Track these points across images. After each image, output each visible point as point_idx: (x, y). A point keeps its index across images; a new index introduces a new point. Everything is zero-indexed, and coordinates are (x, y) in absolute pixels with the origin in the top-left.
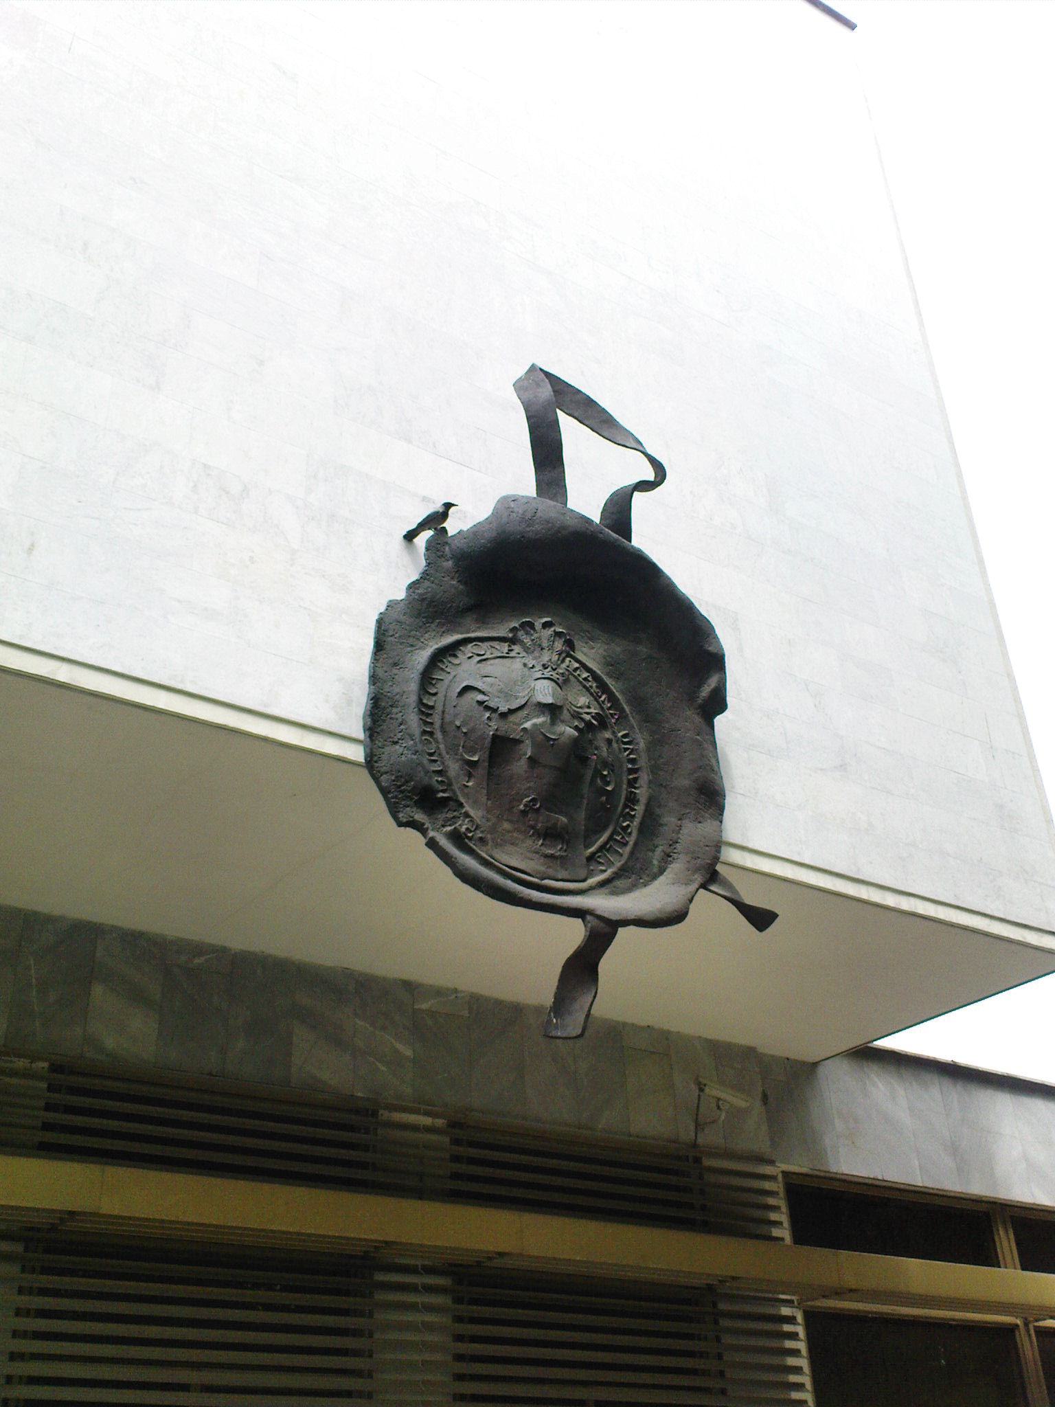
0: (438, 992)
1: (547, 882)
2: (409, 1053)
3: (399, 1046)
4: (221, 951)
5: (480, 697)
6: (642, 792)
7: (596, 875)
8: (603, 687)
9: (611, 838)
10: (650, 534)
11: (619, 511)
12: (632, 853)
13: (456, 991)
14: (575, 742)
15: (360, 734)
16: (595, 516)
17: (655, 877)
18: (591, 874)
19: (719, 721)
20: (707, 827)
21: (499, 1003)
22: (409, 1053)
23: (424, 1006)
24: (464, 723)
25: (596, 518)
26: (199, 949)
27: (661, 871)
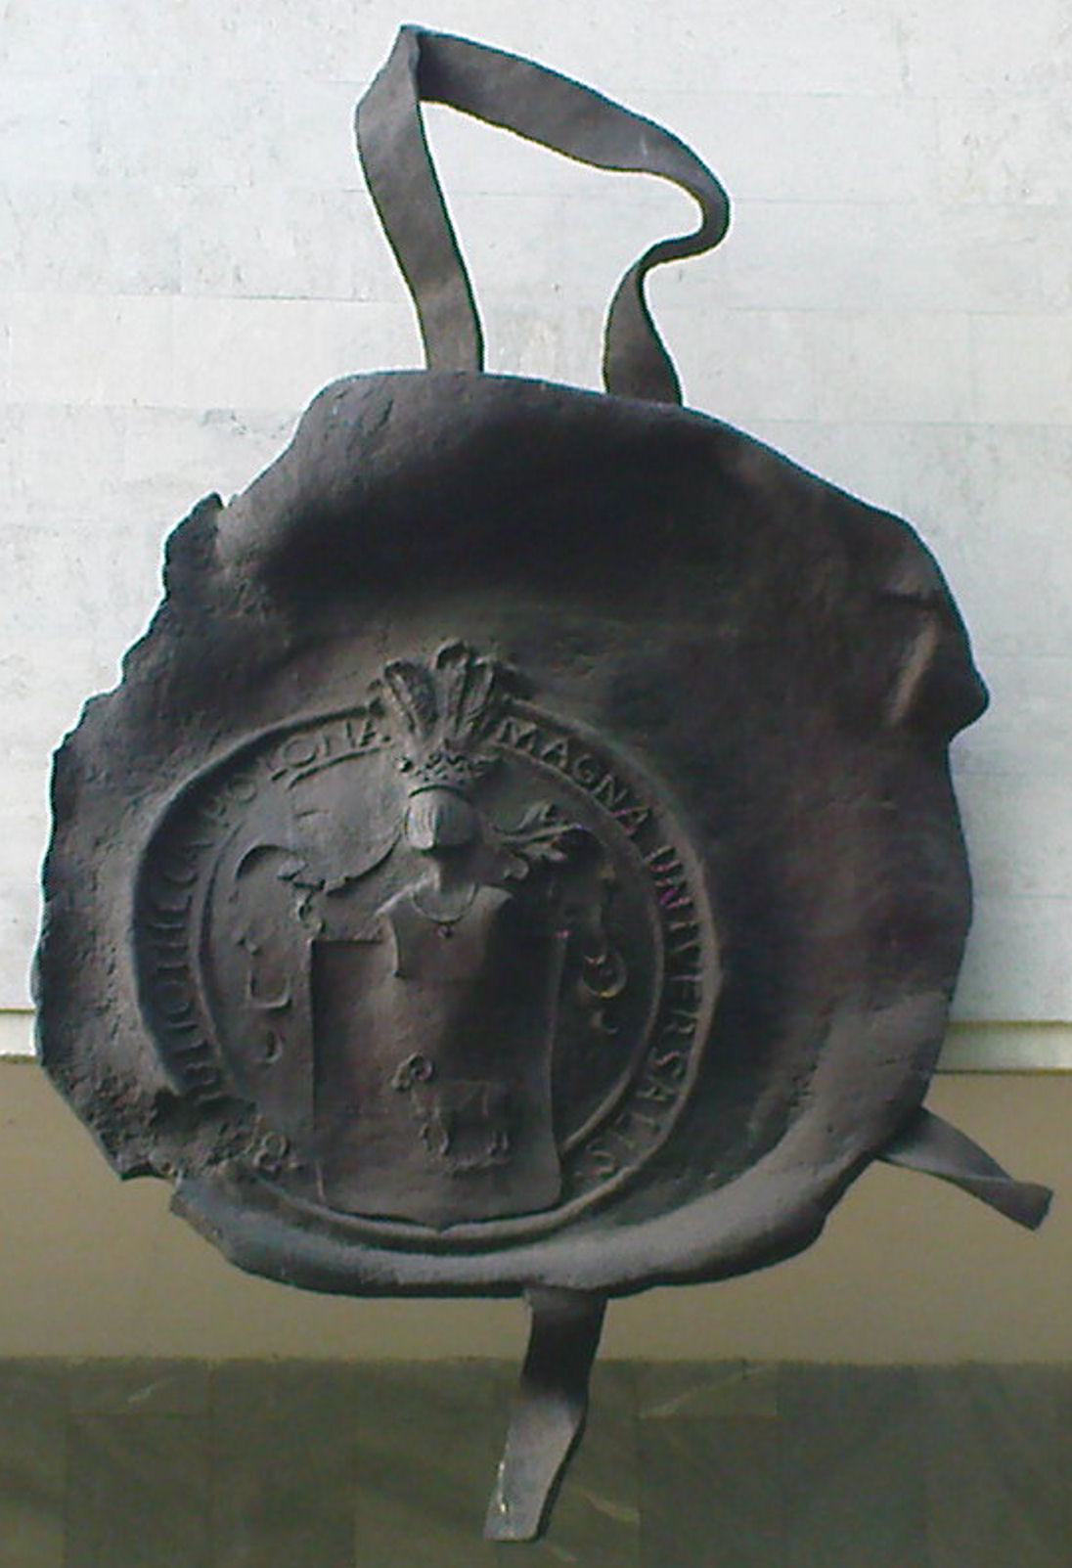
0: (696, 1374)
1: (459, 1231)
2: (630, 1516)
3: (607, 1506)
4: (183, 1371)
5: (287, 866)
6: (709, 979)
7: (593, 1187)
8: (602, 763)
9: (627, 1098)
10: (724, 377)
11: (638, 355)
12: (680, 1125)
13: (744, 1363)
14: (503, 916)
15: (31, 1004)
16: (595, 384)
17: (752, 1158)
18: (569, 1192)
19: (968, 742)
20: (903, 1016)
21: (854, 1375)
22: (630, 1516)
23: (664, 1410)
24: (253, 932)
25: (600, 388)
26: (129, 1374)
27: (770, 1140)
